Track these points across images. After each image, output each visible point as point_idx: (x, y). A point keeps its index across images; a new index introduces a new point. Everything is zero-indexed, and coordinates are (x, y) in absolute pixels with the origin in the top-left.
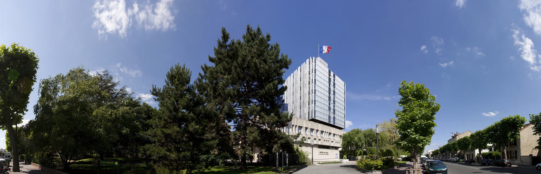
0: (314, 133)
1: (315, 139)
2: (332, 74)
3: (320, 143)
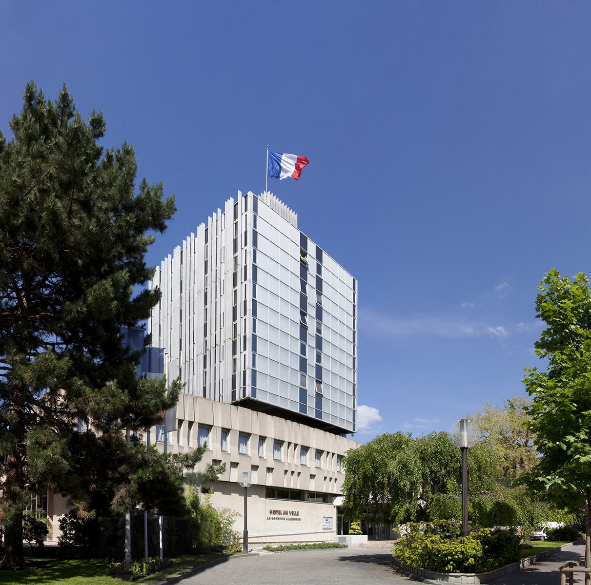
0: (251, 447)
2: (311, 247)
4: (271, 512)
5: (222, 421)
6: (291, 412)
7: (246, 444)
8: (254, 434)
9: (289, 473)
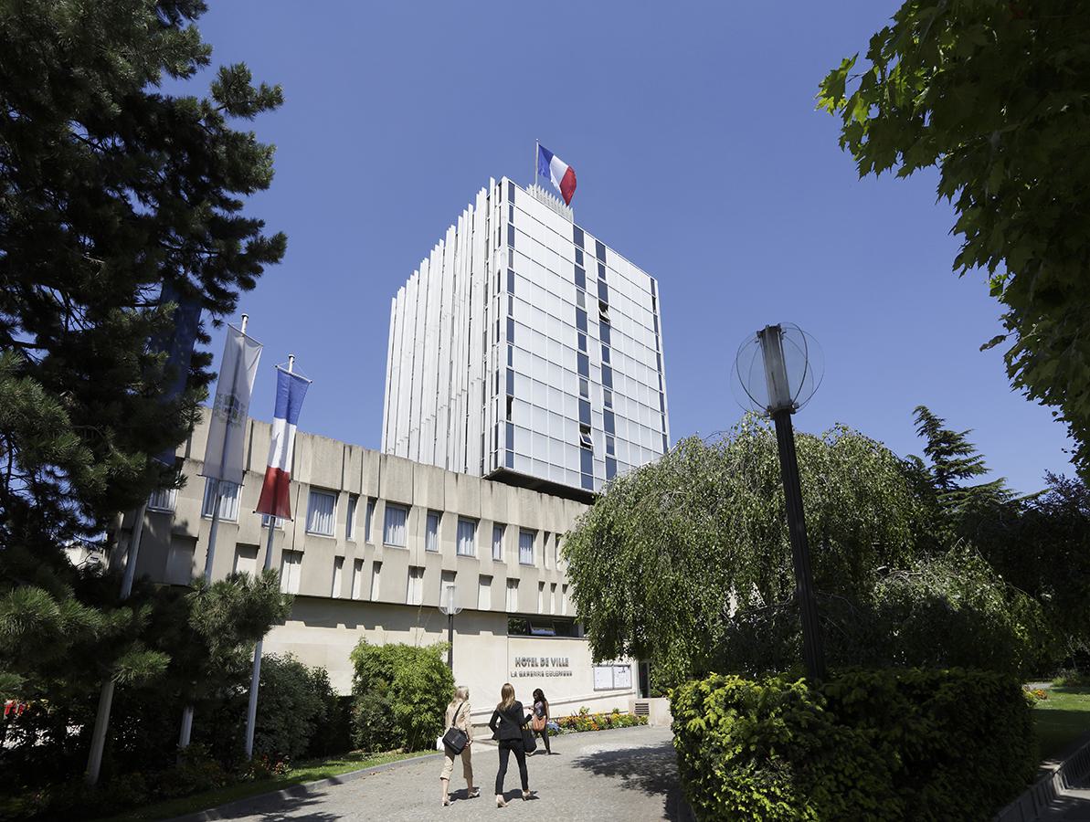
0: (479, 544)
1: (416, 571)
2: (590, 242)
3: (513, 603)
4: (517, 664)
5: (429, 497)
6: (569, 488)
7: (472, 539)
8: (485, 520)
9: (547, 587)
